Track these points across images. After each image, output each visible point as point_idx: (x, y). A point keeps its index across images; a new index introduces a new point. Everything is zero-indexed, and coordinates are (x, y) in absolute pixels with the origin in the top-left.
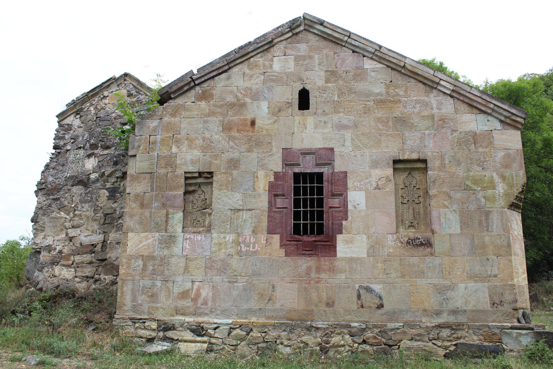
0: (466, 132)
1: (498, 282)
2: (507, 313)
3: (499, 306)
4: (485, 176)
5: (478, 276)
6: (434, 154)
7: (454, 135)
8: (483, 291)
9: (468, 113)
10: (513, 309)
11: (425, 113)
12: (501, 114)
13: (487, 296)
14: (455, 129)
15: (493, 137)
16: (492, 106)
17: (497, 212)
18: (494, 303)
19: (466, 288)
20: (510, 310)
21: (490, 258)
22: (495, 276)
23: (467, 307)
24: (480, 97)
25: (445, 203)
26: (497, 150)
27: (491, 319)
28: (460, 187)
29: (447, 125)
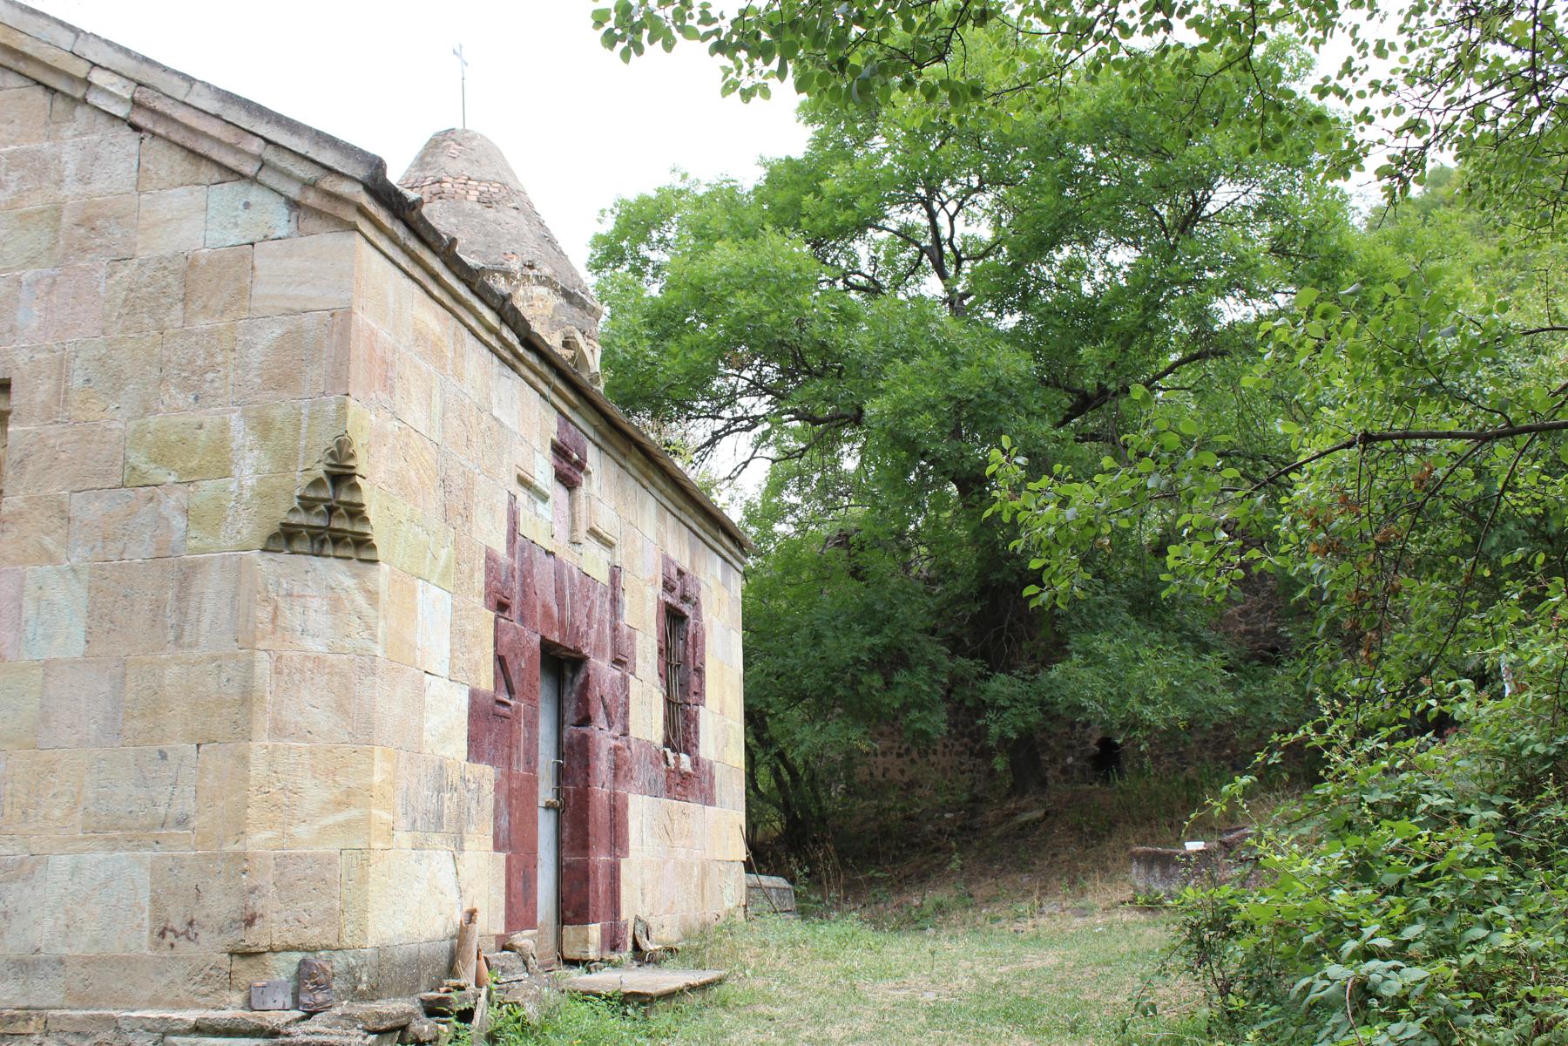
1: (189, 844)
3: (182, 942)
4: (200, 427)
5: (122, 822)
6: (37, 356)
7: (117, 277)
8: (133, 881)
9: (182, 185)
10: (231, 954)
11: (36, 202)
12: (288, 175)
13: (145, 901)
14: (125, 252)
15: (253, 268)
16: (255, 146)
17: (223, 567)
18: (165, 929)
19: (75, 871)
20: (219, 957)
21: (171, 749)
22: (182, 822)
23: (70, 946)
24: (217, 117)
25: (48, 542)
26: (258, 322)
27: (147, 994)
28: (106, 475)
29: (98, 241)
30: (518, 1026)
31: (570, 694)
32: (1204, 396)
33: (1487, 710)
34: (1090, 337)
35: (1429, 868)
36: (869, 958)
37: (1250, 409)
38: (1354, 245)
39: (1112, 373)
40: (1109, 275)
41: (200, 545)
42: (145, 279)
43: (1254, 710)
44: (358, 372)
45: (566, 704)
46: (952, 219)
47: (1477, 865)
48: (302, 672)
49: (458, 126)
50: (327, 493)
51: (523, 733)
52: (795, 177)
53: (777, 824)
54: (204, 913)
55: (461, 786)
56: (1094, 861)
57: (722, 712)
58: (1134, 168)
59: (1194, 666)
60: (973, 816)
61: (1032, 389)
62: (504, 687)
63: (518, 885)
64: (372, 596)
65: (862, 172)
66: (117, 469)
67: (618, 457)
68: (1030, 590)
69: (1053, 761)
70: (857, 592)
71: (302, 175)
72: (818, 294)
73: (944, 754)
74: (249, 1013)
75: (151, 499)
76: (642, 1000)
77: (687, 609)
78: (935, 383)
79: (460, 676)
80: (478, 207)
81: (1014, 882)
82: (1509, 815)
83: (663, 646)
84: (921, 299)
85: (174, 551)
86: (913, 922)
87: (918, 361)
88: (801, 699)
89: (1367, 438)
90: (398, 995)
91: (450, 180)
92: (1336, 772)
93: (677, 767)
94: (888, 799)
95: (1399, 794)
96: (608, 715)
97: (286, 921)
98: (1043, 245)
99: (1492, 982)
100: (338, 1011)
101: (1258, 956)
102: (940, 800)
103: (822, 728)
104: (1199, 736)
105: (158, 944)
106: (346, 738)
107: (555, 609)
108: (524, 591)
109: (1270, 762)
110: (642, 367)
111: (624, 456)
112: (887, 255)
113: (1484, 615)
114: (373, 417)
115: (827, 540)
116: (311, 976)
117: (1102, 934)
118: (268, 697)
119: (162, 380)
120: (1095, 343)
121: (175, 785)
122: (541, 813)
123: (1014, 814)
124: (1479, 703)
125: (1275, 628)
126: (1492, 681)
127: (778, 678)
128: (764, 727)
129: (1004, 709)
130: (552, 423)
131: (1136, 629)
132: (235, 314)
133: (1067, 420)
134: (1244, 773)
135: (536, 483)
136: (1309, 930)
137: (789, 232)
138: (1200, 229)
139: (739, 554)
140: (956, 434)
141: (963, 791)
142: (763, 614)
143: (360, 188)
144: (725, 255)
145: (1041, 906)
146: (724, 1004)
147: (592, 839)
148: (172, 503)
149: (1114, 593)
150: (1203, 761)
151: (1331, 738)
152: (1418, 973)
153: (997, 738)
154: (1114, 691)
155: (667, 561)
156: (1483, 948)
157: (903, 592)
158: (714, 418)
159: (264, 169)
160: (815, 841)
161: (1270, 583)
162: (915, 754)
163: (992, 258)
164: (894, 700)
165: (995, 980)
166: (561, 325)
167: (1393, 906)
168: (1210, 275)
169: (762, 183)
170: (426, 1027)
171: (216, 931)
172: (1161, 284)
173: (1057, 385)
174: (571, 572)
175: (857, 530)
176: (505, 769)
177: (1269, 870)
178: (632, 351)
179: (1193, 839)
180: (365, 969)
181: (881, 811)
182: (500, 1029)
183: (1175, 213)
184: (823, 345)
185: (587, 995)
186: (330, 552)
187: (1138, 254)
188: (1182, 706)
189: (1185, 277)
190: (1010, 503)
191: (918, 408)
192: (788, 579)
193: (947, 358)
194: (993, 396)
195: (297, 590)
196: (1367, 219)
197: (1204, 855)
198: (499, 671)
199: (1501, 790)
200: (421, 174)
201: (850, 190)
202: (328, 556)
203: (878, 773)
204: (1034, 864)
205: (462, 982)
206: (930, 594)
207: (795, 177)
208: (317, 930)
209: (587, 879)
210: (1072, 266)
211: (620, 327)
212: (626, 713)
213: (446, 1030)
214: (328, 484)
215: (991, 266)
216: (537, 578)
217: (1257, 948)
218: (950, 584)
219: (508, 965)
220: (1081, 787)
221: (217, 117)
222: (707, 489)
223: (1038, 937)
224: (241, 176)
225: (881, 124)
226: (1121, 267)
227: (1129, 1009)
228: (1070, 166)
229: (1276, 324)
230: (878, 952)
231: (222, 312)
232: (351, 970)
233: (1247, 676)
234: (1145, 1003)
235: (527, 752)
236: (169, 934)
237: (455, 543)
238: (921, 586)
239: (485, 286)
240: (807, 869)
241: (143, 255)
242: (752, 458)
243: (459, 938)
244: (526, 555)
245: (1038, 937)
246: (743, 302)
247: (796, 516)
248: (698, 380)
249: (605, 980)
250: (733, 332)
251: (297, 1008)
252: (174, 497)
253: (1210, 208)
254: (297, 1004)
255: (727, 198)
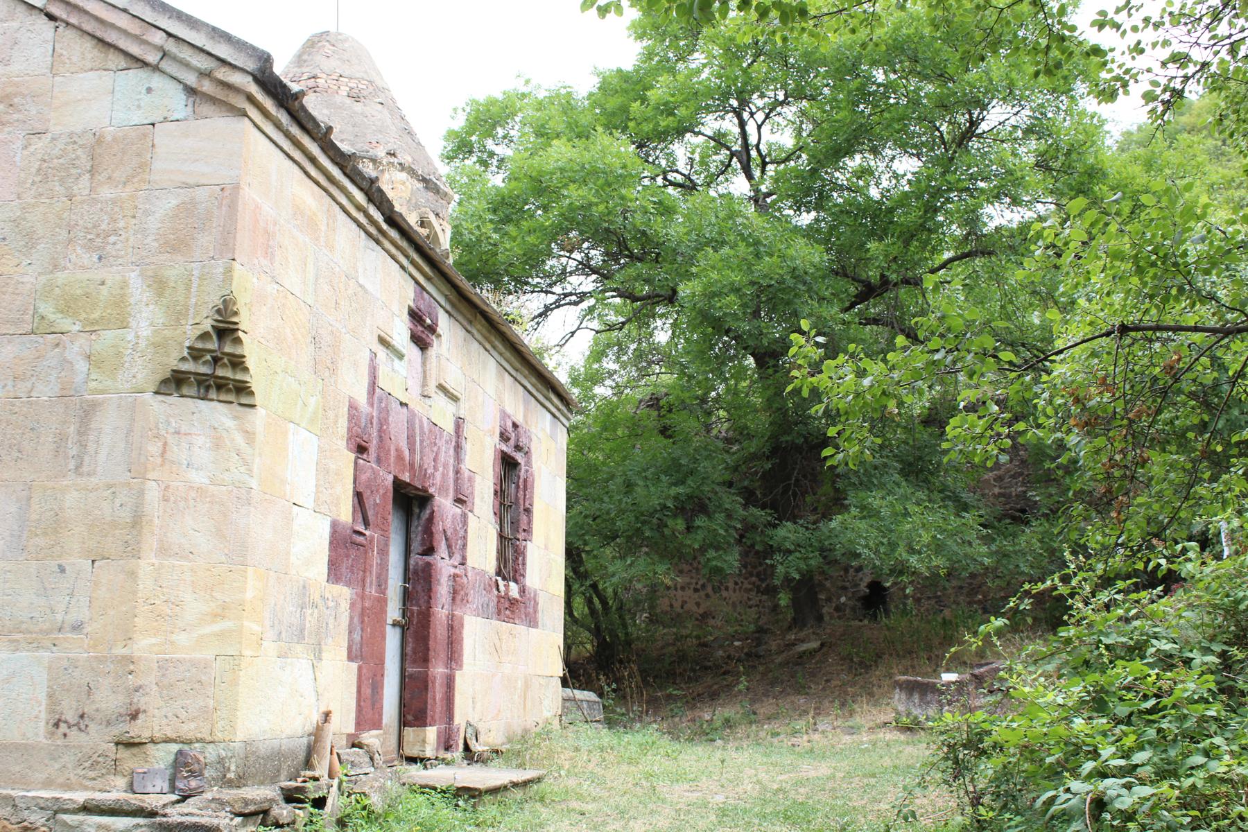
0: (71, 135)
2: (95, 757)
3: (73, 733)
4: (103, 283)
5: (24, 626)
7: (32, 149)
9: (92, 69)
10: (117, 744)
12: (187, 65)
13: (42, 696)
14: (39, 127)
15: (153, 146)
16: (158, 38)
18: (59, 720)
20: (105, 746)
22: (77, 627)
24: (125, 11)
26: (157, 193)
27: (41, 777)
28: (16, 323)
29: (16, 116)
30: (364, 813)
31: (417, 527)
32: (972, 289)
33: (1210, 569)
34: (876, 234)
35: (1158, 703)
36: (668, 764)
37: (1011, 302)
38: (1107, 164)
39: (894, 267)
40: (894, 181)
41: (100, 387)
42: (56, 152)
43: (1004, 562)
44: (243, 241)
45: (413, 536)
46: (759, 127)
47: (1196, 702)
48: (186, 500)
49: (333, 30)
50: (213, 345)
51: (375, 559)
52: (625, 86)
53: (589, 646)
54: (94, 707)
55: (321, 603)
56: (862, 687)
57: (546, 548)
58: (920, 89)
59: (954, 522)
60: (758, 645)
61: (824, 278)
62: (360, 519)
63: (367, 691)
64: (249, 436)
65: (683, 84)
66: (28, 317)
67: (465, 323)
68: (827, 452)
69: (829, 600)
70: (665, 448)
71: (199, 65)
72: (640, 188)
73: (735, 591)
74: (131, 796)
75: (57, 345)
76: (471, 793)
77: (519, 457)
78: (740, 270)
79: (324, 509)
80: (348, 101)
81: (792, 702)
82: (1225, 660)
83: (499, 488)
84: (728, 196)
85: (77, 391)
86: (705, 734)
87: (726, 250)
88: (614, 538)
89: (1124, 329)
90: (262, 783)
91: (324, 76)
92: (1078, 617)
93: (507, 594)
94: (685, 627)
95: (1131, 639)
96: (449, 547)
97: (166, 717)
98: (838, 152)
99: (1207, 803)
100: (209, 795)
101: (1005, 774)
102: (731, 630)
103: (633, 563)
104: (955, 583)
105: (53, 734)
106: (223, 559)
107: (407, 453)
108: (381, 437)
109: (1021, 608)
110: (486, 247)
111: (470, 322)
112: (702, 157)
113: (1215, 485)
114: (255, 280)
115: (640, 401)
116: (186, 764)
117: (867, 750)
118: (156, 521)
119: (70, 241)
120: (881, 239)
121: (71, 595)
122: (389, 629)
123: (794, 645)
124: (1203, 563)
125: (1025, 492)
126: (1213, 544)
127: (594, 520)
128: (581, 562)
129: (790, 552)
130: (410, 290)
131: (905, 488)
132: (136, 185)
133: (852, 306)
134: (997, 614)
135: (394, 343)
136: (1052, 752)
137: (617, 133)
138: (974, 144)
139: (566, 411)
140: (756, 314)
141: (750, 623)
142: (583, 464)
143: (250, 79)
144: (561, 152)
145: (815, 724)
146: (542, 800)
147: (432, 653)
148: (76, 349)
149: (888, 457)
150: (958, 604)
151: (1075, 588)
152: (1147, 791)
153: (782, 578)
154: (885, 541)
155: (504, 415)
156: (1202, 774)
157: (705, 449)
158: (547, 292)
159: (165, 59)
160: (621, 662)
161: (1022, 453)
162: (709, 589)
163: (792, 163)
164: (695, 541)
165: (775, 786)
166: (417, 207)
167: (1126, 734)
168: (981, 185)
169: (595, 90)
170: (285, 812)
171: (104, 723)
172: (938, 192)
173: (846, 276)
174: (421, 421)
175: (667, 394)
176: (359, 591)
177: (1018, 700)
178: (477, 233)
179: (948, 670)
180: (233, 760)
181: (679, 638)
182: (348, 815)
183: (953, 130)
184: (644, 233)
185: (425, 789)
186: (214, 397)
187: (920, 164)
188: (943, 556)
189: (961, 185)
190: (810, 379)
191: (725, 291)
192: (605, 435)
193: (752, 249)
194: (790, 281)
195: (184, 429)
196: (1117, 142)
197: (960, 684)
198: (357, 505)
199: (1219, 638)
200: (299, 70)
201: (672, 99)
202: (212, 400)
203: (677, 605)
204: (810, 688)
205: (317, 774)
206: (727, 452)
207: (625, 86)
208: (193, 725)
209: (426, 688)
210: (862, 172)
211: (466, 212)
212: (465, 545)
213: (302, 815)
214: (215, 337)
215: (795, 169)
216: (392, 425)
217: (1005, 767)
218: (745, 444)
219: (357, 760)
220: (852, 623)
221: (125, 11)
222: (540, 354)
223: (811, 751)
224: (145, 64)
225: (701, 42)
226: (905, 175)
227: (892, 815)
228: (864, 85)
229: (1044, 225)
230: (676, 759)
231: (125, 183)
232: (221, 761)
233: (1000, 533)
234: (905, 810)
235: (379, 576)
236: (62, 725)
237: (323, 392)
238: (720, 444)
239: (355, 169)
240: (614, 686)
241: (55, 129)
242: (578, 328)
243: (315, 735)
244: (383, 405)
245: (811, 751)
246: (575, 194)
247: (614, 380)
248: (534, 260)
249: (440, 775)
250: (566, 219)
251: (173, 792)
252: (77, 344)
253: (984, 127)
254: (173, 789)
255: (567, 105)
